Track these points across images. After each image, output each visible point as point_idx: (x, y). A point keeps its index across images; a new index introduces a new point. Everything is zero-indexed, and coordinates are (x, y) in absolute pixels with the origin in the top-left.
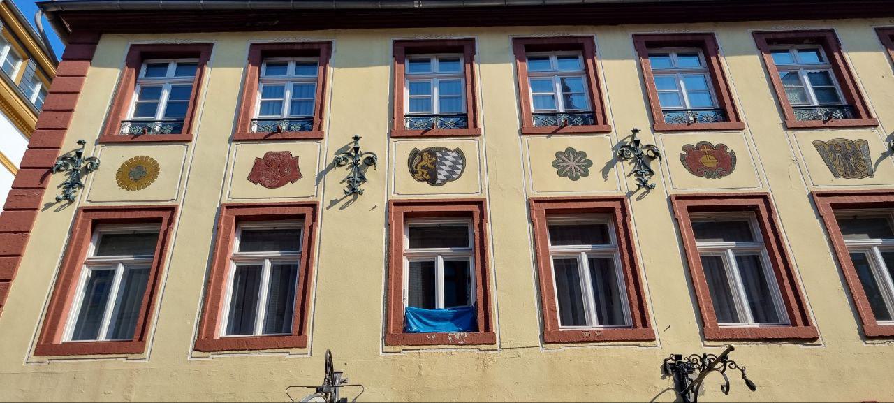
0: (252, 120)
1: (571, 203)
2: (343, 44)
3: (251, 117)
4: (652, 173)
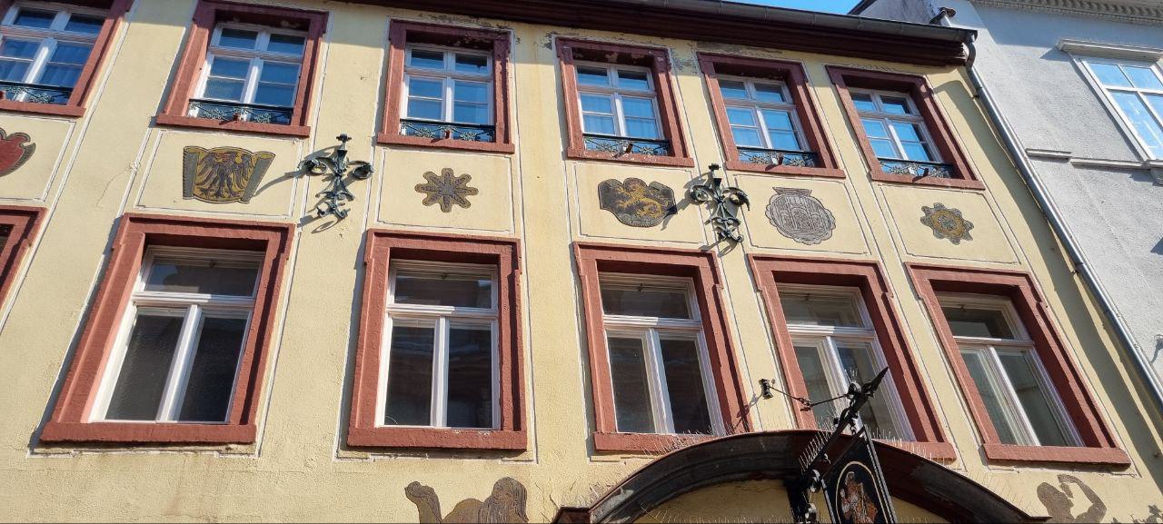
0: (191, 100)
1: (623, 253)
2: (339, 19)
3: (189, 97)
4: (737, 222)
